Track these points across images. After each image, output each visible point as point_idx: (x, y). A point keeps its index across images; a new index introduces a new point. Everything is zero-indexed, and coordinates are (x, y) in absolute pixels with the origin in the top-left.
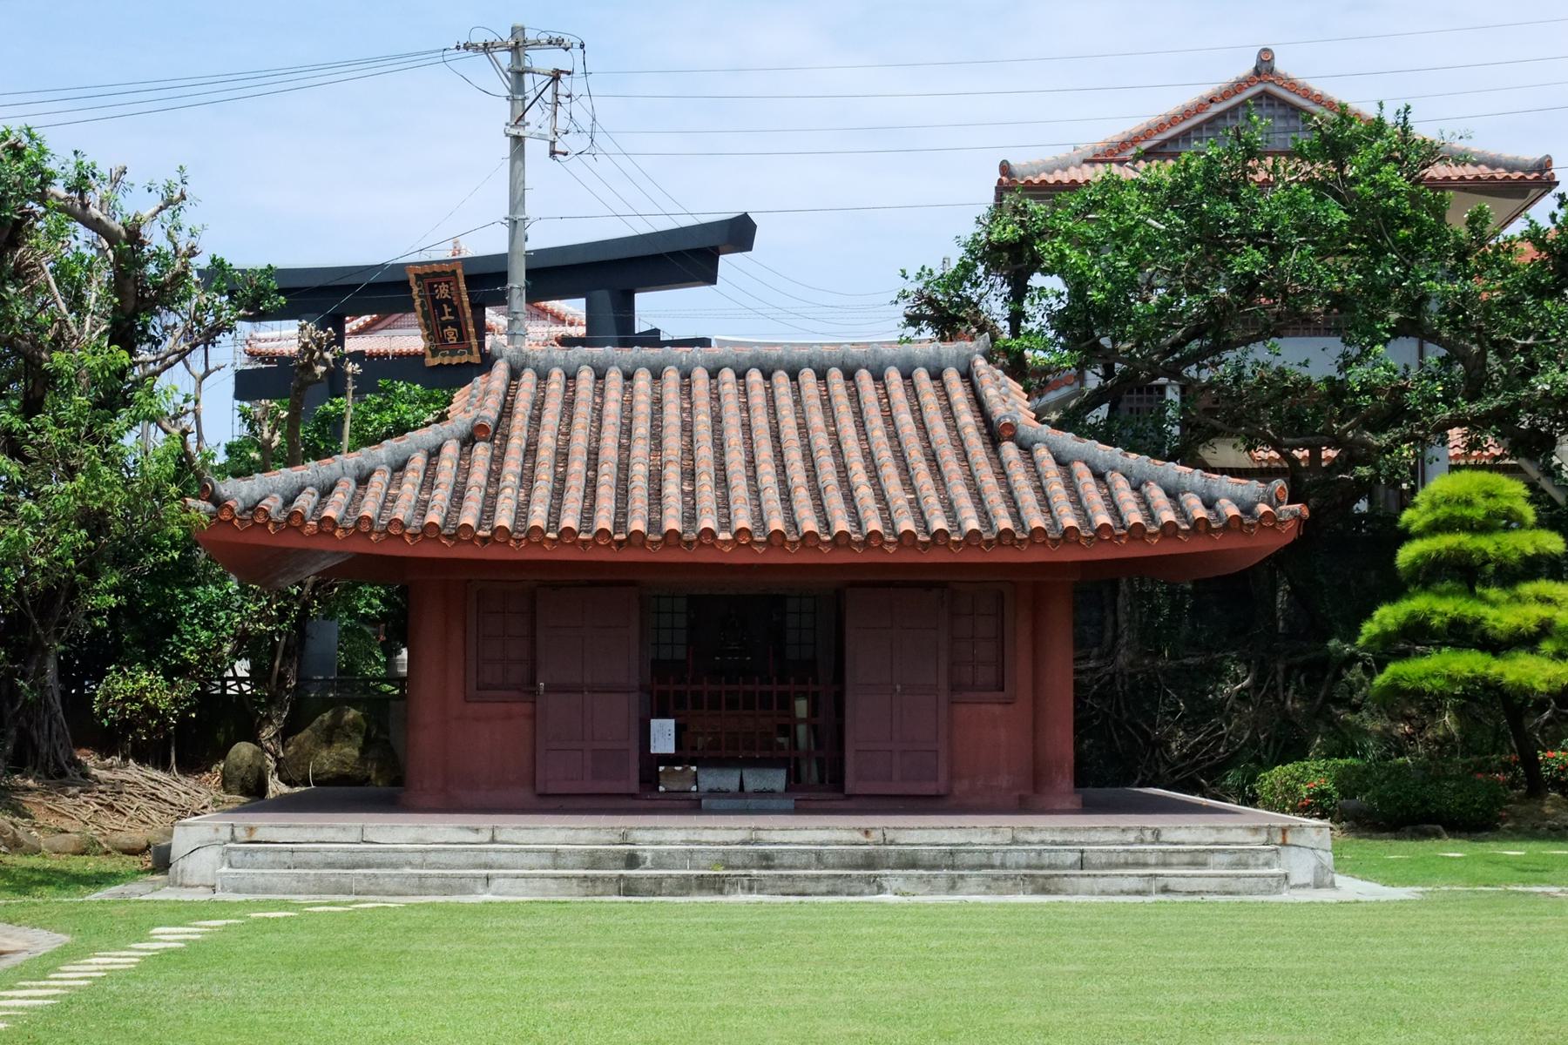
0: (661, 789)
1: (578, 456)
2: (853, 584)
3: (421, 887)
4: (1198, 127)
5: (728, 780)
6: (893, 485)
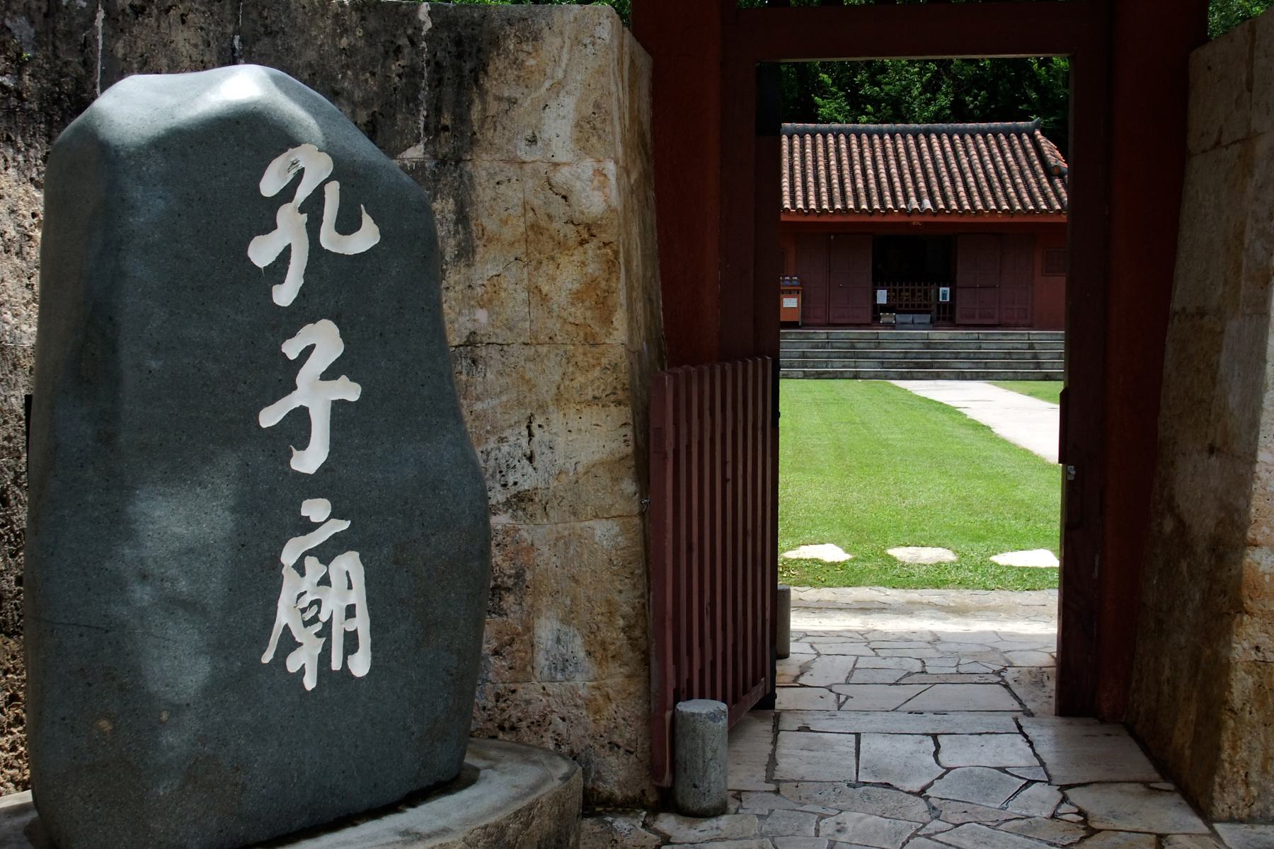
5: (909, 318)
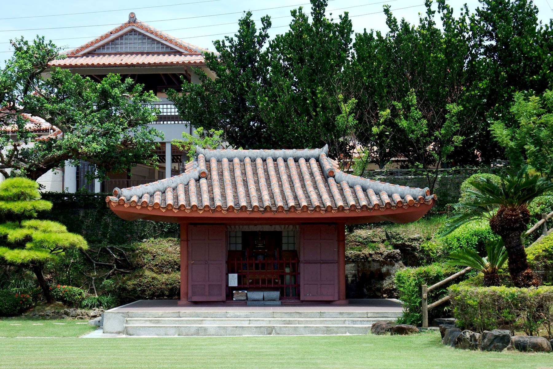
0: (234, 299)
1: (285, 181)
2: (191, 224)
3: (327, 331)
4: (107, 44)
6: (310, 189)
